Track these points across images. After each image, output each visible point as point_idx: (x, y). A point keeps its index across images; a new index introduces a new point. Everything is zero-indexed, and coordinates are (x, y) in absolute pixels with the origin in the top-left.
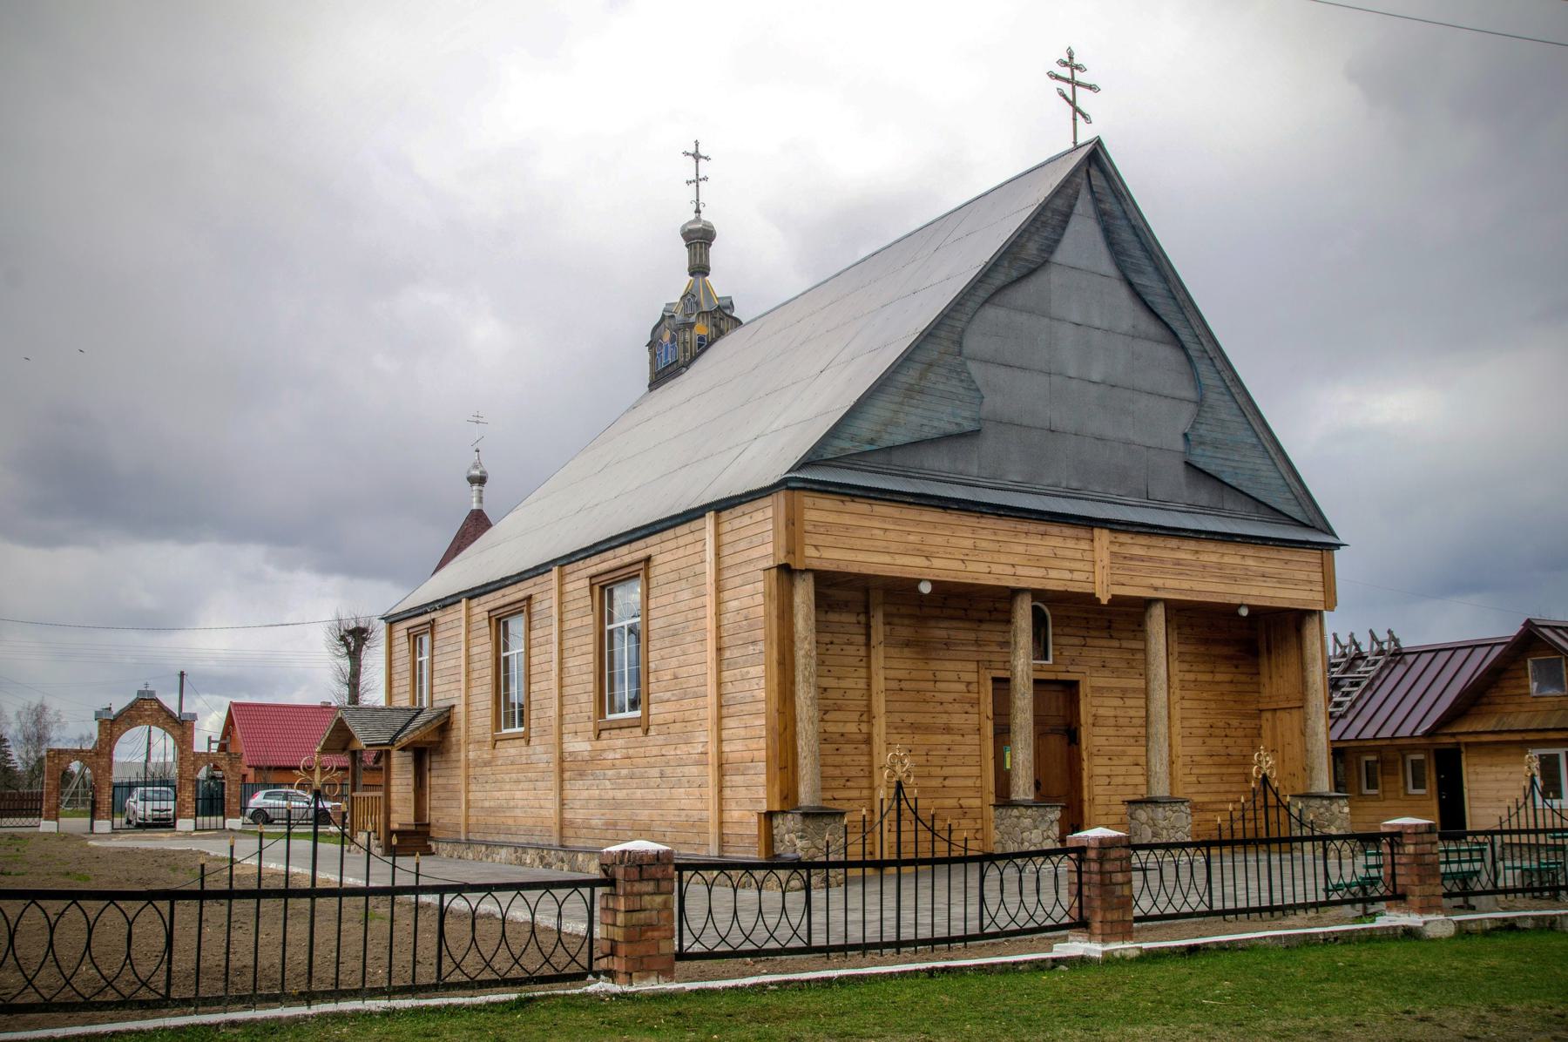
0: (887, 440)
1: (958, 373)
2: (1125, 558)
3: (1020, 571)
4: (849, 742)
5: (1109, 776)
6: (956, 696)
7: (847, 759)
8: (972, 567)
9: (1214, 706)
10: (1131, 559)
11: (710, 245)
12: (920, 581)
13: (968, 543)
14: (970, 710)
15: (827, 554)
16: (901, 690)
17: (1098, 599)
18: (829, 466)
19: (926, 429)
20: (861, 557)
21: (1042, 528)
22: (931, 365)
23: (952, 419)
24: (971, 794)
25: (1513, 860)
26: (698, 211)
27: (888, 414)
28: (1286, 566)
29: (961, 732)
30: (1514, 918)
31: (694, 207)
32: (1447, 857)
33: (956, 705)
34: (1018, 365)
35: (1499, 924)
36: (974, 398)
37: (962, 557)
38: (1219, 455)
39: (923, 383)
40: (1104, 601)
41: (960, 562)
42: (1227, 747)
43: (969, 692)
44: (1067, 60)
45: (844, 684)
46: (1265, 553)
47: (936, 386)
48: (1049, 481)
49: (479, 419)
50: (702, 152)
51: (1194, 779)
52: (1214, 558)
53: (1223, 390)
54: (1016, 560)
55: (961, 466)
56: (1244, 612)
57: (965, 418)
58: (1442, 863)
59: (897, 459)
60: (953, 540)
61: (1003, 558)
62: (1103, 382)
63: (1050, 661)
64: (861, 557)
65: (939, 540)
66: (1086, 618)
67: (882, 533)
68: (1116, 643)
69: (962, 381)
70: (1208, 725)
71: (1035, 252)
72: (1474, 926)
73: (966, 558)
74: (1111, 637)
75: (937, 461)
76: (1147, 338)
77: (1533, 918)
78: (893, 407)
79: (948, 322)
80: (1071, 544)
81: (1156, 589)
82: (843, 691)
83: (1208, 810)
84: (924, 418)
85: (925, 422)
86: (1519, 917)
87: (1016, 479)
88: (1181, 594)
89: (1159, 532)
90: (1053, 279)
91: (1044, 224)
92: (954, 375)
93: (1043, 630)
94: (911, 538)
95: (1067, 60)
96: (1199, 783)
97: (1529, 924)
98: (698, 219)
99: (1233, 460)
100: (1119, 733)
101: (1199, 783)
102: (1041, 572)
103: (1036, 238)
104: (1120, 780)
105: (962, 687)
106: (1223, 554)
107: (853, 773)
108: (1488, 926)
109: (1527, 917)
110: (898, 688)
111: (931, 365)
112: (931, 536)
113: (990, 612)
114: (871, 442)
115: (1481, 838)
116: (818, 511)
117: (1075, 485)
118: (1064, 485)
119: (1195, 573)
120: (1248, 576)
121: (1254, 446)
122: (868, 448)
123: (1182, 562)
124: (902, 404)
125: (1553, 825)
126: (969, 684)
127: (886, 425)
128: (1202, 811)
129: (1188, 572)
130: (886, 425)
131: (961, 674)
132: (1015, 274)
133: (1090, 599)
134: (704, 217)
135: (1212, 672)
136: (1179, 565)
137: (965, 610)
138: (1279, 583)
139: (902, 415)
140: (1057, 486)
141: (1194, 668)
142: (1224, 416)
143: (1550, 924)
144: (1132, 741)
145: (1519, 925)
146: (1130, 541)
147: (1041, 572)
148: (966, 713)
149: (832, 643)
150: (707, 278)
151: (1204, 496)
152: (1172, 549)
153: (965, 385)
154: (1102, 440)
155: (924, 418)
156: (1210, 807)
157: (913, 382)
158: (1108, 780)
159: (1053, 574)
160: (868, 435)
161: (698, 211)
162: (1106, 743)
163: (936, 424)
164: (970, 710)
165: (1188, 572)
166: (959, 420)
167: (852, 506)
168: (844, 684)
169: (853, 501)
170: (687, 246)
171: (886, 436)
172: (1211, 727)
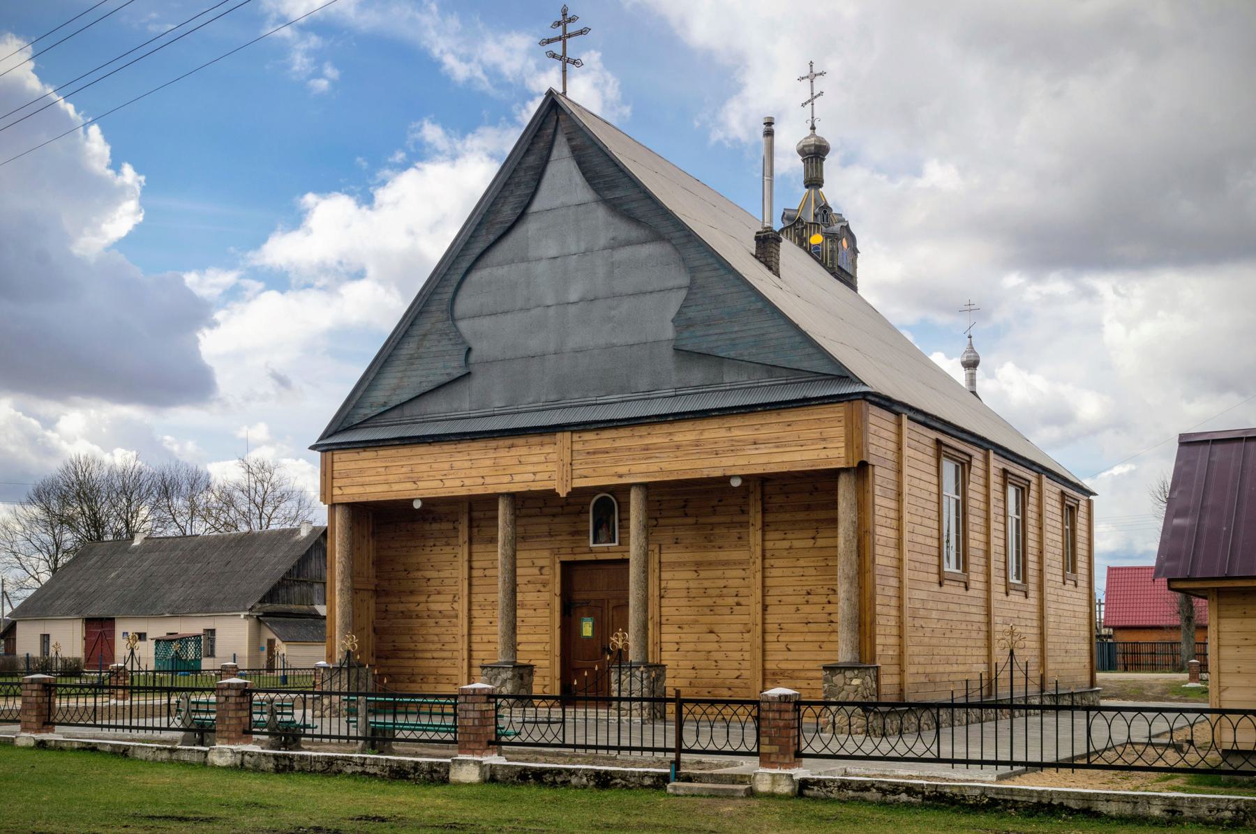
0: (395, 401)
1: (446, 334)
2: (588, 453)
3: (488, 480)
4: (444, 617)
5: (677, 643)
6: (529, 578)
7: (443, 629)
8: (448, 483)
9: (814, 572)
10: (594, 453)
11: (823, 159)
12: (412, 500)
13: (447, 466)
14: (542, 589)
15: (347, 491)
16: (485, 576)
17: (558, 494)
18: (361, 428)
19: (424, 384)
20: (368, 489)
21: (508, 442)
22: (425, 335)
23: (443, 371)
24: (541, 656)
25: (131, 705)
26: (813, 128)
27: (395, 381)
28: (789, 428)
29: (533, 607)
30: (96, 744)
31: (810, 125)
32: (197, 707)
33: (530, 586)
34: (500, 311)
35: (84, 746)
36: (460, 350)
37: (442, 478)
38: (711, 332)
39: (421, 350)
40: (563, 494)
41: (440, 482)
42: (830, 614)
43: (541, 574)
44: (568, 16)
45: (442, 574)
46: (755, 420)
47: (431, 350)
48: (531, 399)
49: (972, 307)
50: (806, 72)
51: (782, 646)
52: (691, 436)
53: (717, 266)
54: (483, 472)
55: (455, 405)
56: (736, 483)
57: (455, 368)
58: (279, 714)
59: (408, 411)
60: (435, 466)
61: (474, 472)
62: (581, 300)
63: (617, 544)
64: (368, 489)
65: (424, 468)
66: (658, 501)
67: (383, 469)
68: (691, 520)
69: (450, 339)
70: (805, 592)
71: (510, 212)
72: (65, 745)
73: (444, 477)
74: (686, 515)
75: (437, 406)
76: (629, 243)
77: (111, 745)
78: (399, 375)
79: (437, 297)
80: (536, 450)
81: (621, 476)
82: (441, 580)
83: (797, 678)
84: (422, 376)
85: (424, 379)
86: (100, 743)
87: (500, 405)
88: (648, 477)
89: (619, 424)
90: (530, 227)
91: (518, 184)
92: (444, 337)
93: (612, 517)
94: (404, 470)
95: (568, 16)
96: (789, 650)
97: (108, 748)
98: (813, 135)
99: (731, 333)
100: (691, 604)
101: (789, 650)
102: (507, 479)
103: (511, 199)
104: (691, 647)
105: (536, 571)
106: (730, 428)
107: (447, 640)
108: (76, 746)
109: (107, 744)
110: (482, 575)
111: (425, 335)
112: (419, 466)
113: (562, 507)
114: (385, 404)
115: (293, 696)
116: (344, 462)
117: (553, 397)
118: (543, 400)
119: (665, 455)
120: (735, 447)
121: (760, 311)
122: (383, 409)
123: (650, 446)
124: (405, 370)
125: (967, 714)
126: (542, 568)
127: (395, 390)
128: (791, 678)
129: (657, 455)
130: (395, 390)
131: (535, 561)
132: (492, 238)
133: (550, 494)
134: (817, 132)
135: (813, 538)
136: (647, 450)
137: (540, 508)
138: (778, 447)
139: (405, 379)
140: (537, 402)
141: (789, 536)
142: (719, 292)
143: (124, 751)
144: (706, 610)
145: (99, 748)
146: (596, 437)
147: (507, 479)
148: (539, 591)
149: (434, 545)
150: (820, 189)
151: (697, 375)
152: (641, 436)
153: (453, 342)
154: (581, 351)
155: (422, 376)
156: (802, 674)
157: (413, 352)
158: (677, 647)
159: (517, 478)
160: (382, 400)
161: (813, 128)
162: (677, 613)
163: (431, 378)
164: (542, 589)
165: (657, 455)
166: (449, 371)
167: (382, 453)
168: (442, 574)
169: (365, 451)
170: (803, 161)
171: (395, 398)
172: (809, 594)
